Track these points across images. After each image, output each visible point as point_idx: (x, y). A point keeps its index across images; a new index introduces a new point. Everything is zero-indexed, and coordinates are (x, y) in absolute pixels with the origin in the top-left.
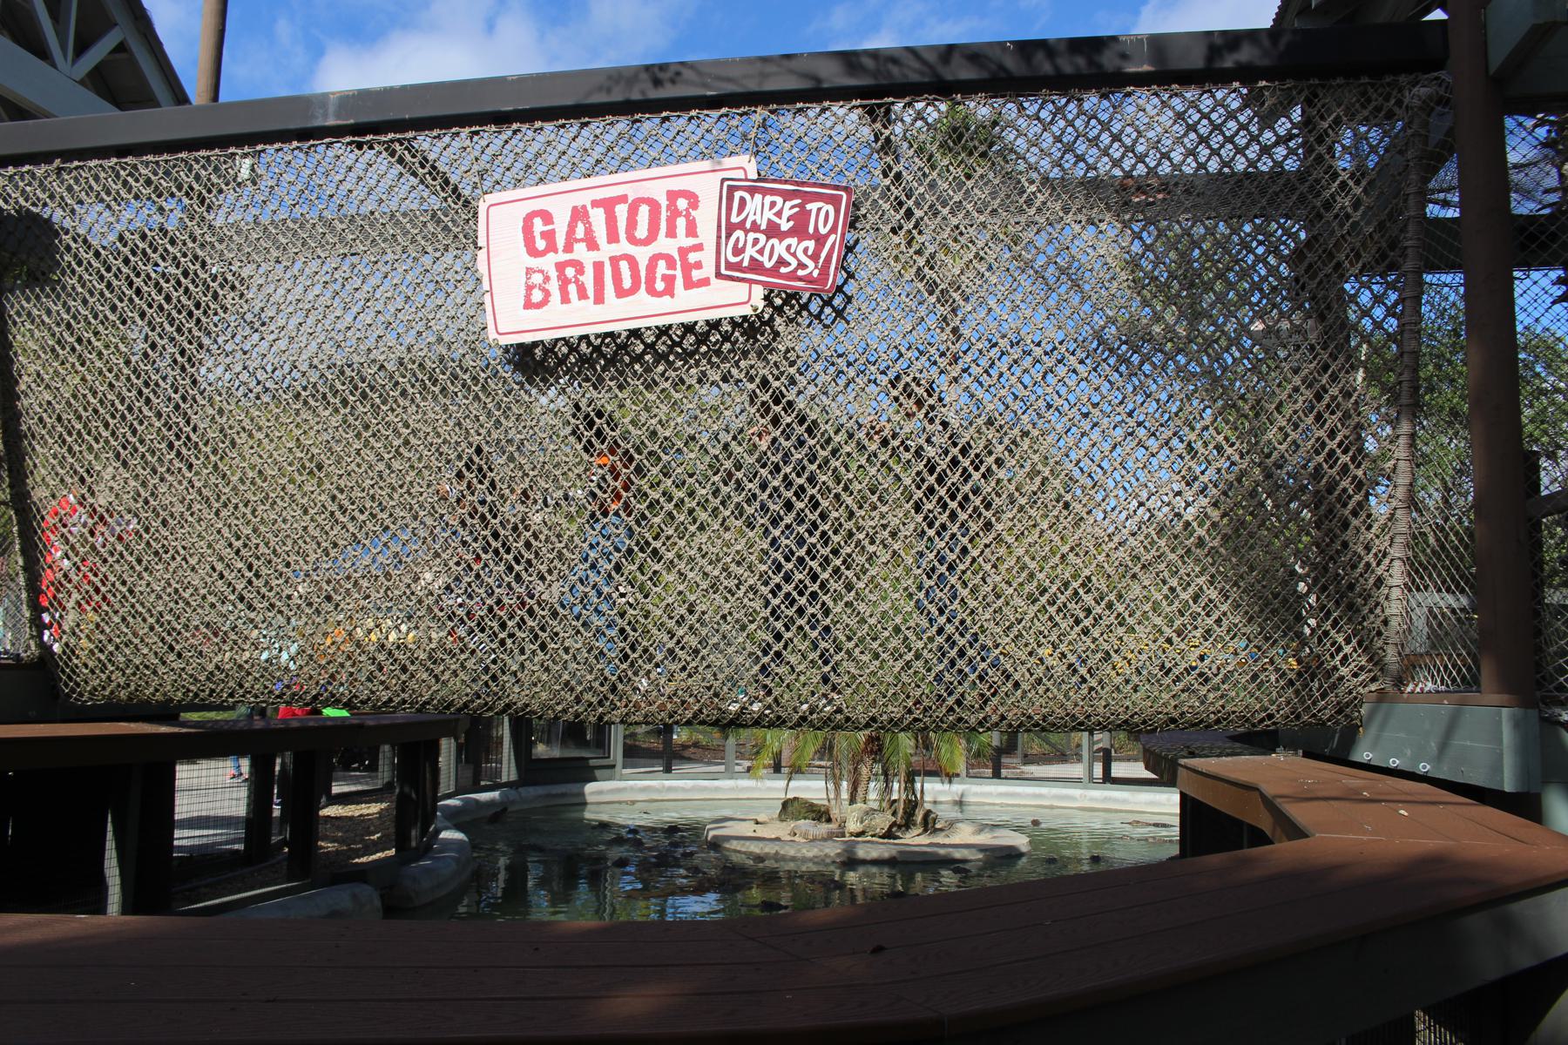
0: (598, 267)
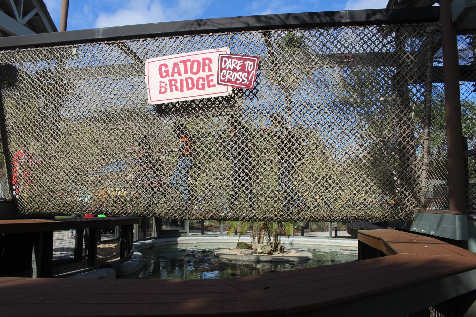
0: (182, 81)
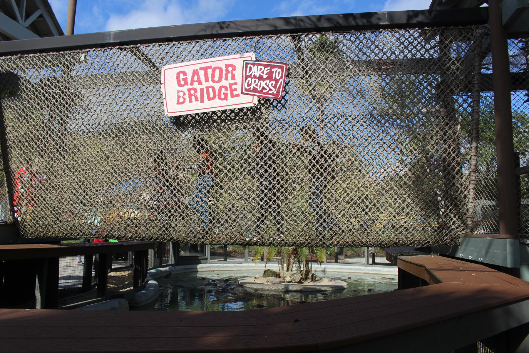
0: (202, 90)
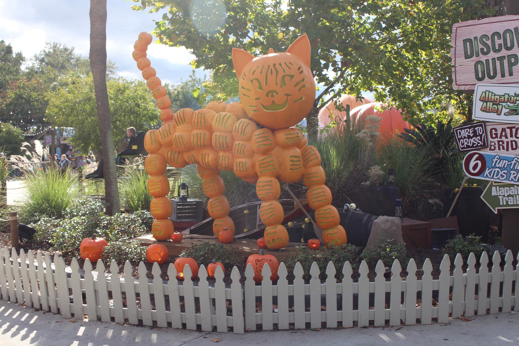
0: (508, 143)
